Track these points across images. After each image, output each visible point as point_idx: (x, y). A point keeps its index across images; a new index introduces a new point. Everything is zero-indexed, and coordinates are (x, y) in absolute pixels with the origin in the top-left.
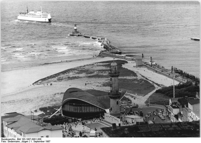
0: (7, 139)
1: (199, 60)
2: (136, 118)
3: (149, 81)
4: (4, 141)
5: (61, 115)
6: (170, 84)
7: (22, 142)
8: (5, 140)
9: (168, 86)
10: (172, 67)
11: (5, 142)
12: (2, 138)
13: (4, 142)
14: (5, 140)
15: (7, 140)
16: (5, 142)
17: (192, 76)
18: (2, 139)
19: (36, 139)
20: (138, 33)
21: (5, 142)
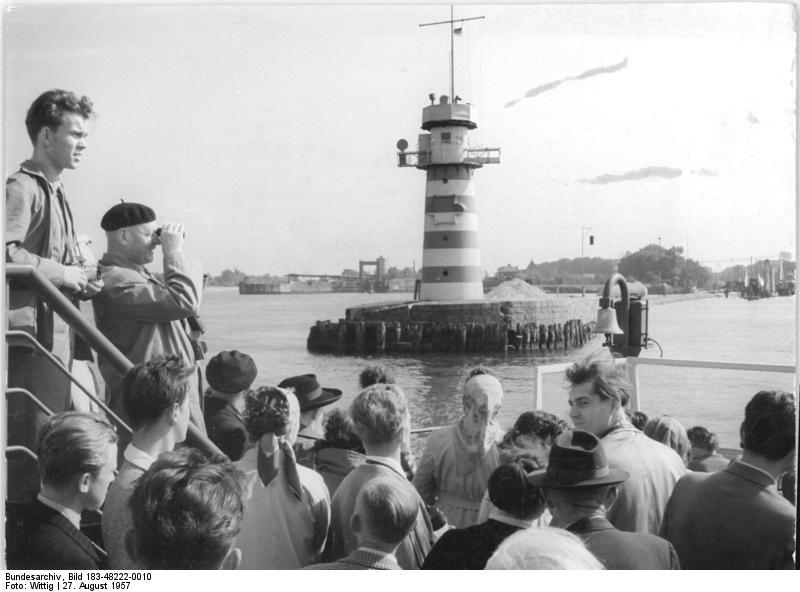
0: (28, 577)
4: (14, 582)
6: (52, 281)
8: (19, 582)
12: (8, 571)
14: (19, 582)
18: (8, 576)
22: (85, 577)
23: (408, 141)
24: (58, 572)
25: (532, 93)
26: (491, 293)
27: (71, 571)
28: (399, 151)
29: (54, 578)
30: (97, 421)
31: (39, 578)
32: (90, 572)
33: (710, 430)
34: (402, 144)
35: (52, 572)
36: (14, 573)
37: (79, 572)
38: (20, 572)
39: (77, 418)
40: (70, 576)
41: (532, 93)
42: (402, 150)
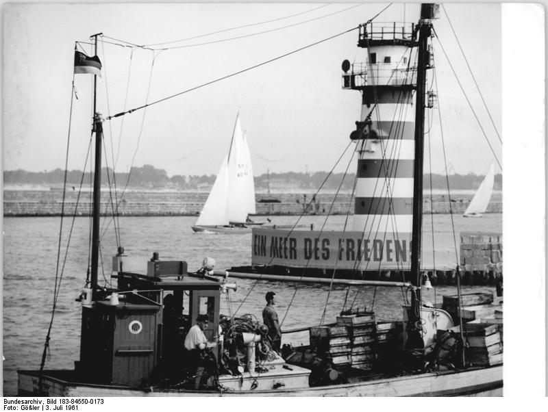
0: (19, 402)
1: (502, 319)
2: (62, 215)
3: (281, 229)
4: (10, 405)
5: (256, 229)
6: (315, 321)
7: (57, 411)
8: (13, 405)
9: (155, 168)
10: (156, 256)
11: (13, 411)
12: (5, 398)
13: (10, 411)
14: (13, 405)
15: (18, 405)
16: (15, 408)
17: (393, 94)
18: (5, 401)
19: (76, 408)
20: (62, 275)
21: (15, 408)
22: (58, 401)
23: (348, 59)
24: (40, 399)
25: (123, 114)
26: (196, 211)
27: (48, 398)
28: (343, 72)
29: (37, 403)
30: (14, 322)
31: (27, 402)
32: (62, 398)
33: (182, 175)
34: (413, 24)
35: (36, 398)
36: (9, 399)
37: (54, 398)
38: (14, 399)
39: (108, 184)
40: (48, 401)
41: (123, 114)
42: (346, 72)
